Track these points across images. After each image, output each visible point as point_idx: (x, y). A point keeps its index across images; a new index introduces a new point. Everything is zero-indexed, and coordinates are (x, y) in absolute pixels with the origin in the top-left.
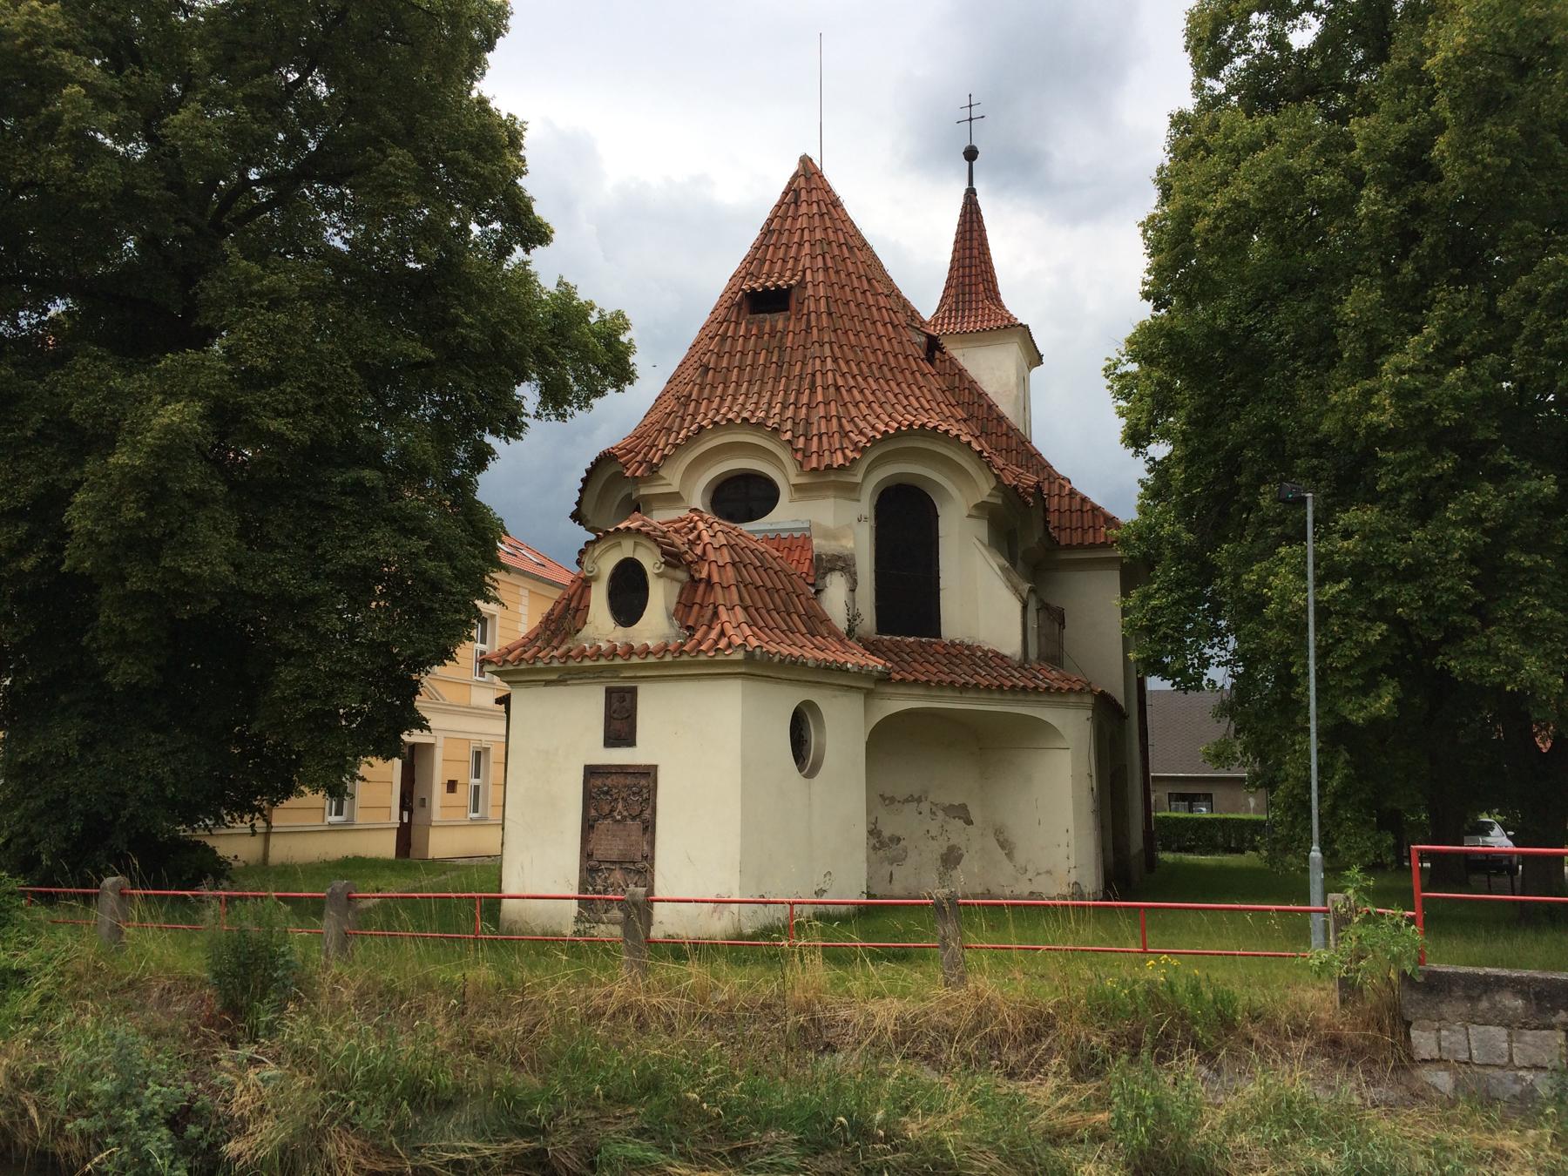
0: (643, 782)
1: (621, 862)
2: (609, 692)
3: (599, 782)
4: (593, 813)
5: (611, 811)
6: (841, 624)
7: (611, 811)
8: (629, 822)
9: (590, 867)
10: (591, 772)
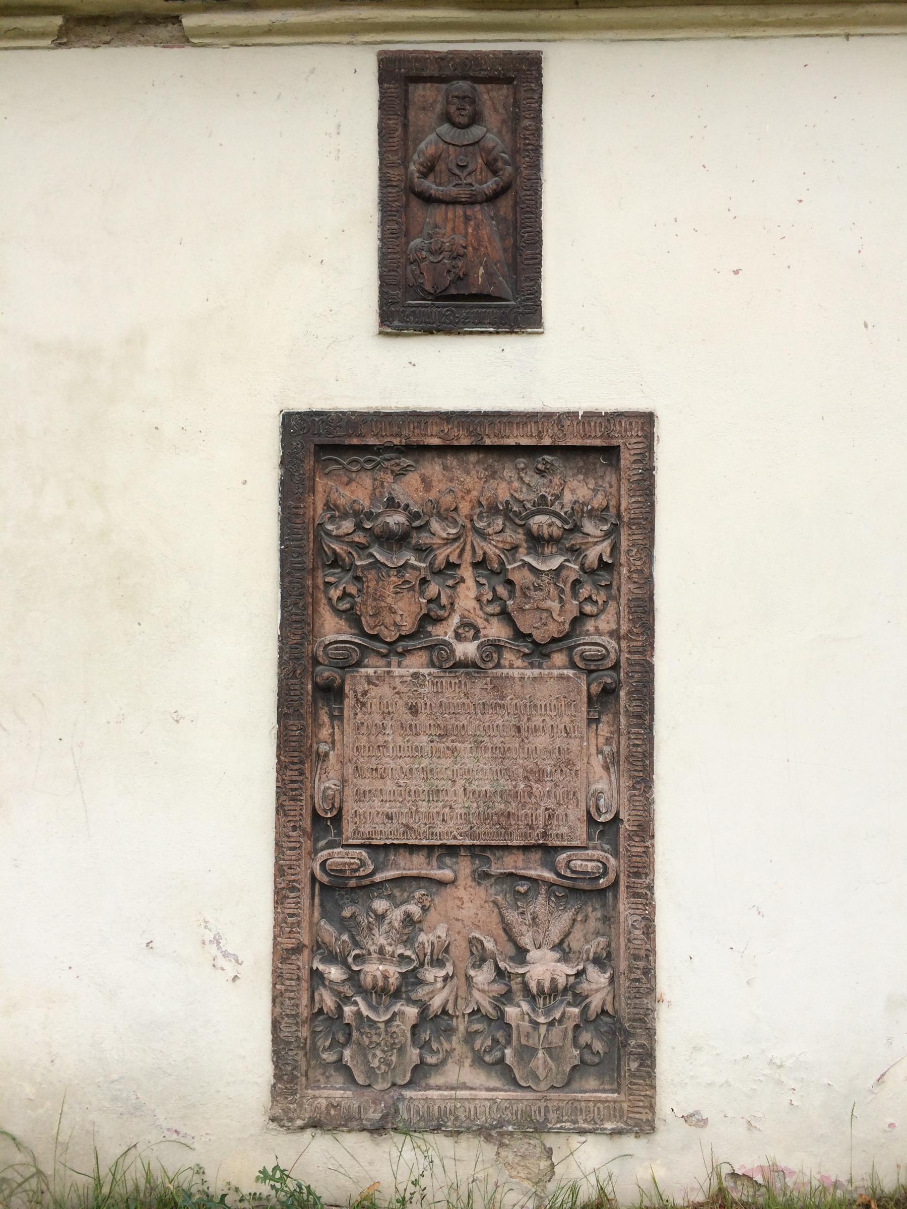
0: (578, 489)
1: (478, 852)
2: (399, 78)
3: (358, 491)
4: (332, 629)
5: (428, 619)
6: (602, 940)
7: (428, 619)
8: (514, 667)
9: (330, 873)
10: (317, 444)
